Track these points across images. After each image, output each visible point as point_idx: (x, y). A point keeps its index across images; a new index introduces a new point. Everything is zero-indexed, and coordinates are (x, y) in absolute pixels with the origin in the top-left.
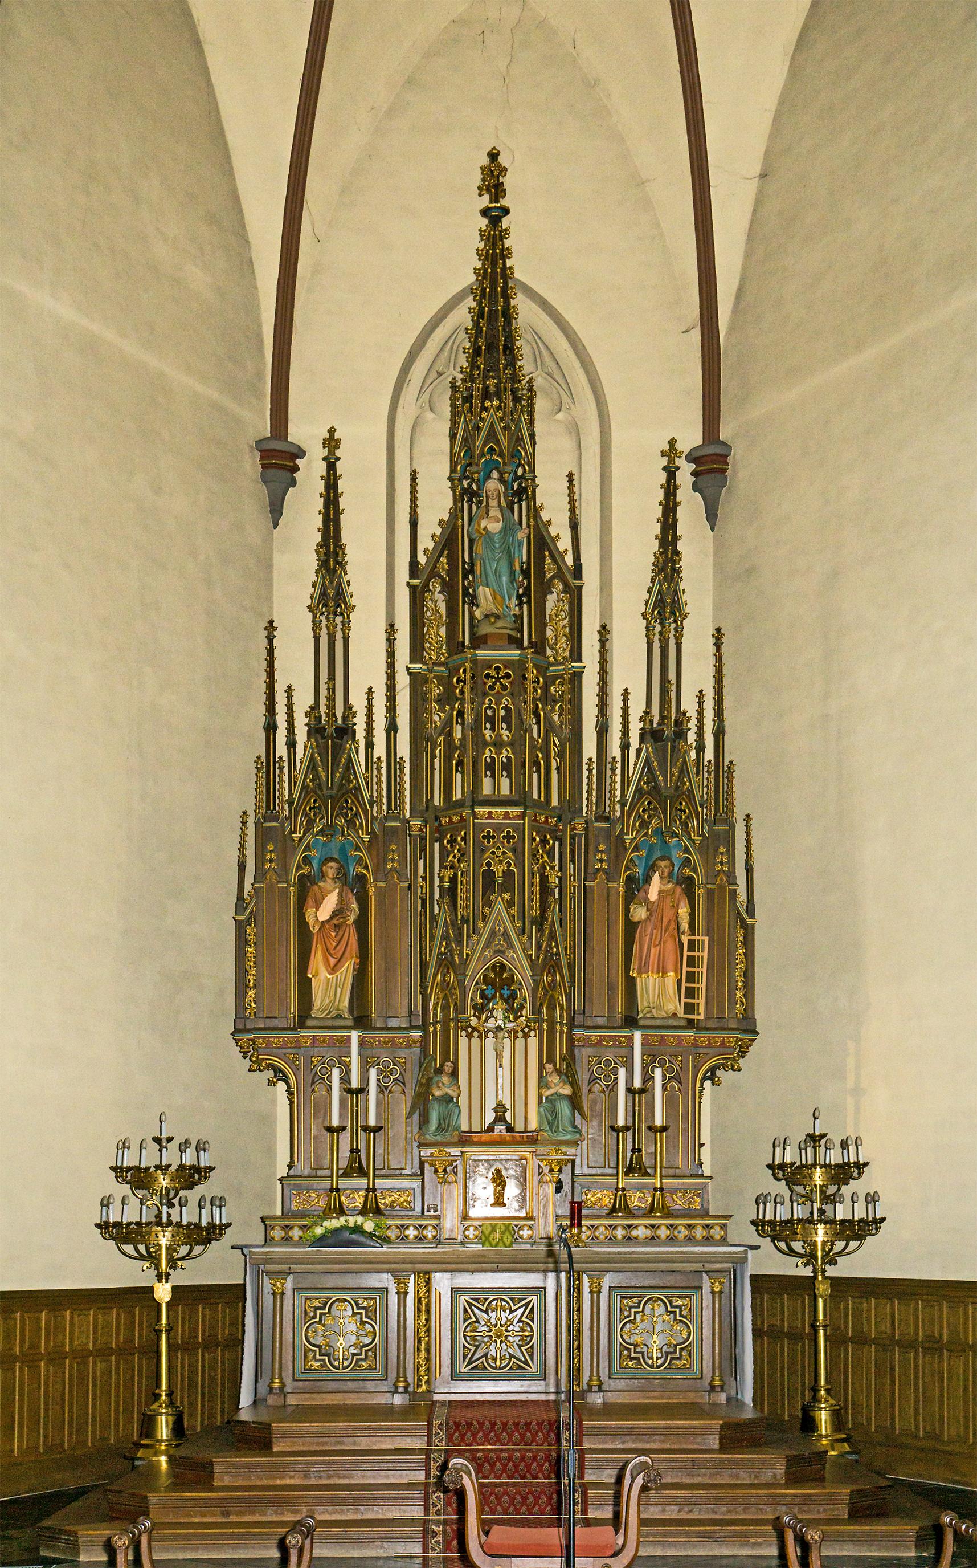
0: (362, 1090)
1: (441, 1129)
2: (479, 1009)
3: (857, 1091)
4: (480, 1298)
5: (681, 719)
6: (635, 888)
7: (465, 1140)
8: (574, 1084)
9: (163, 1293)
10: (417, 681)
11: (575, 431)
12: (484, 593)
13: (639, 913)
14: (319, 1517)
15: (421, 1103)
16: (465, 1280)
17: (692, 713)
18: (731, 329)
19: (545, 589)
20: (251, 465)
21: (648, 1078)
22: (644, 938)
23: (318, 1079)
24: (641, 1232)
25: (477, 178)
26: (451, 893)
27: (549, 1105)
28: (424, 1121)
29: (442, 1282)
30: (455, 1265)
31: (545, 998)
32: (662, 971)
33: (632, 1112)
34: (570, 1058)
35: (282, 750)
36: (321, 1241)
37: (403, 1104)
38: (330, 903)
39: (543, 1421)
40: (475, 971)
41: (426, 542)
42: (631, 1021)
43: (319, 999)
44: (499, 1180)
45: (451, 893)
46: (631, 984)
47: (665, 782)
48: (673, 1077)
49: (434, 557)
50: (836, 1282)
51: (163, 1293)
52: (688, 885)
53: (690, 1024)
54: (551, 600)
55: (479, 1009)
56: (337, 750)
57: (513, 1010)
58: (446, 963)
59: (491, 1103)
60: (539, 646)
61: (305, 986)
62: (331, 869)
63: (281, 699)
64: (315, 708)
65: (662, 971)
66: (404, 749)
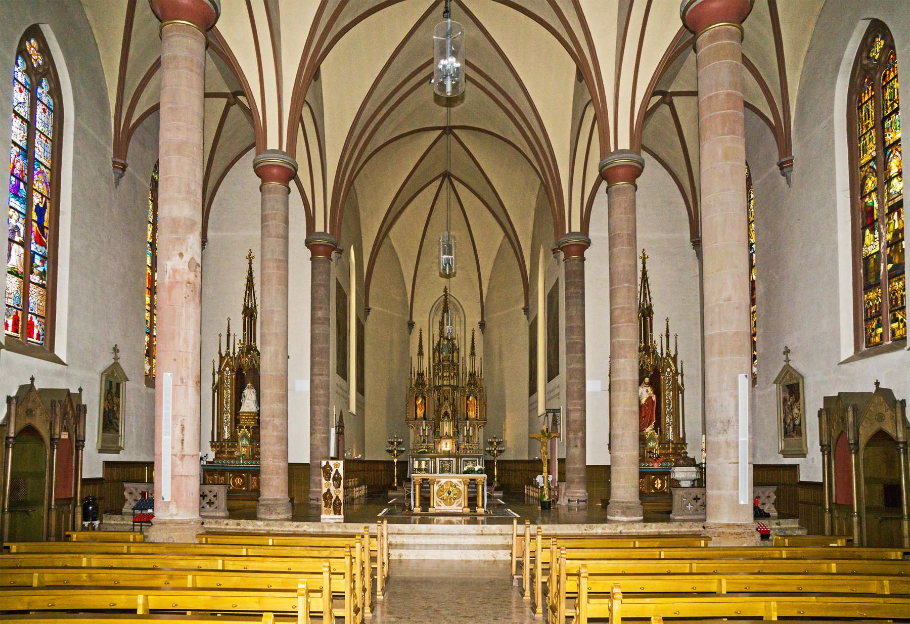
0: (425, 430)
1: (438, 436)
2: (443, 418)
3: (505, 430)
4: (443, 462)
5: (475, 372)
6: (468, 398)
7: (441, 438)
8: (458, 429)
9: (395, 460)
10: (434, 366)
11: (460, 317)
12: (444, 353)
13: (469, 402)
14: (754, 255)
15: (434, 433)
16: (441, 459)
17: (477, 371)
18: (486, 302)
19: (453, 352)
20: (406, 326)
21: (469, 428)
22: (469, 406)
23: (418, 428)
24: (468, 452)
25: (443, 290)
26: (439, 400)
27: (454, 433)
28: (435, 435)
29: (438, 459)
30: (439, 457)
31: (453, 416)
32: (472, 411)
33: (467, 434)
34: (457, 425)
35: (413, 377)
36: (419, 453)
37: (431, 432)
38: (420, 401)
39: (400, 484)
40: (443, 412)
41: (435, 345)
42: (467, 419)
43: (418, 416)
44: (446, 444)
45: (439, 400)
46: (467, 413)
47: (473, 382)
48: (474, 428)
49: (436, 347)
50: (498, 461)
51: (395, 460)
52: (476, 398)
53: (477, 420)
54: (455, 354)
55: (443, 418)
56: (422, 378)
57: (449, 418)
58: (438, 411)
59: (445, 432)
60: (453, 361)
61: (416, 413)
62: (420, 395)
63: (413, 369)
64: (418, 371)
65: (472, 411)
66: (432, 377)
